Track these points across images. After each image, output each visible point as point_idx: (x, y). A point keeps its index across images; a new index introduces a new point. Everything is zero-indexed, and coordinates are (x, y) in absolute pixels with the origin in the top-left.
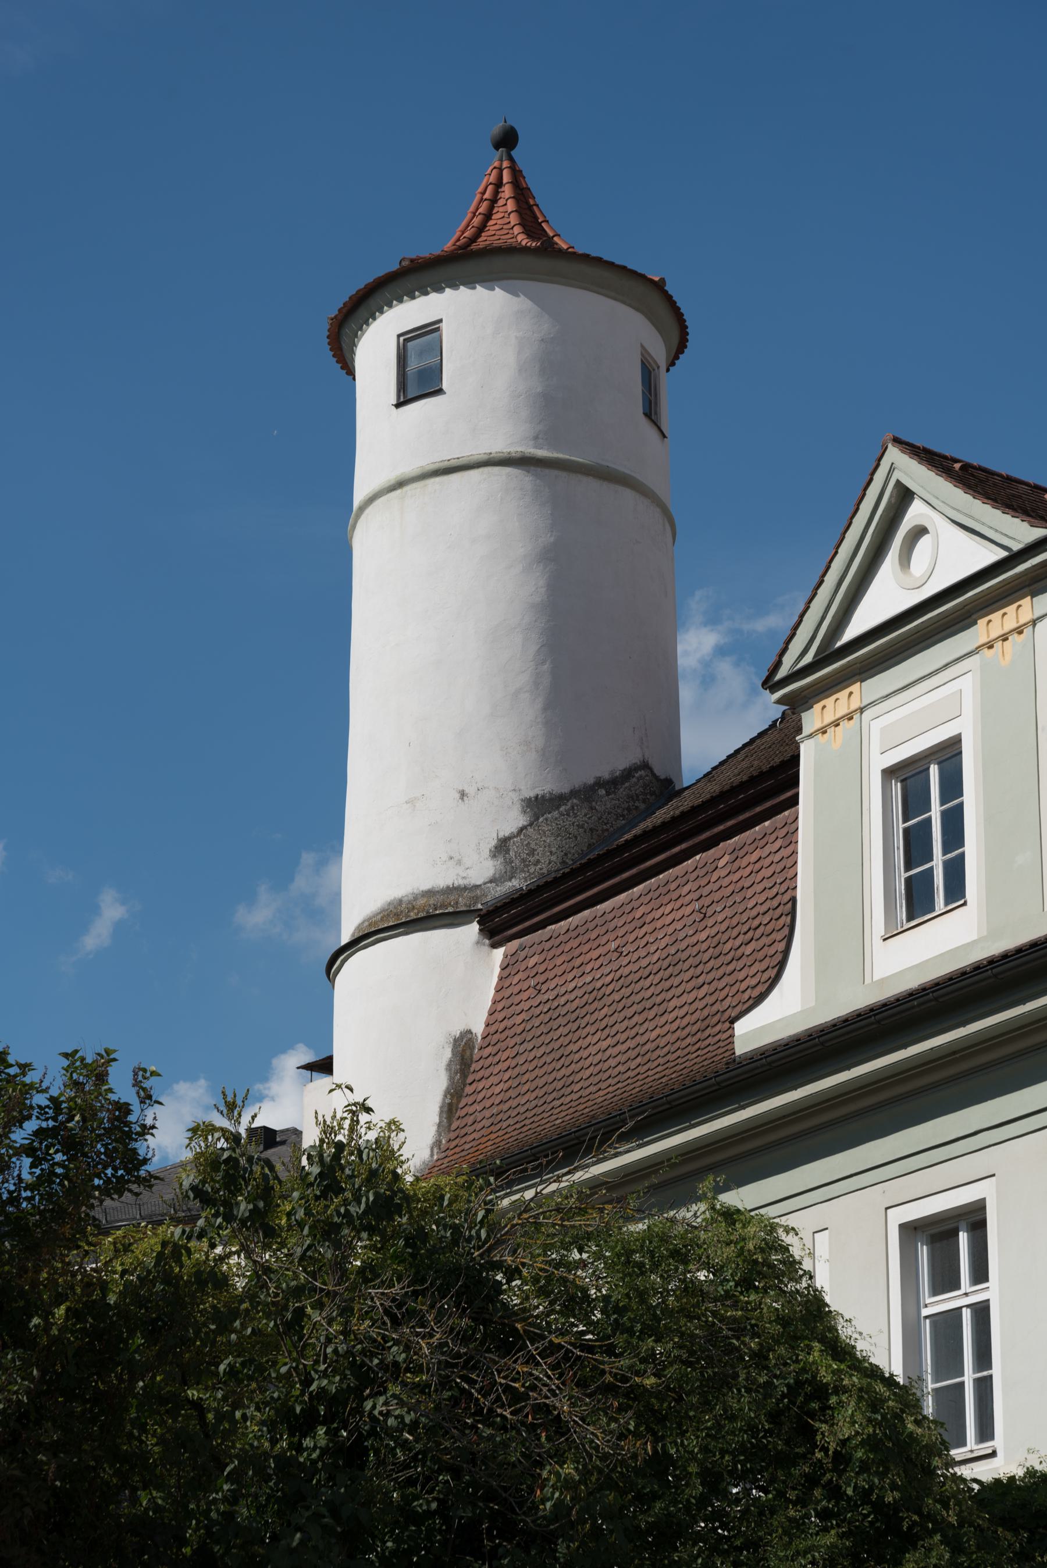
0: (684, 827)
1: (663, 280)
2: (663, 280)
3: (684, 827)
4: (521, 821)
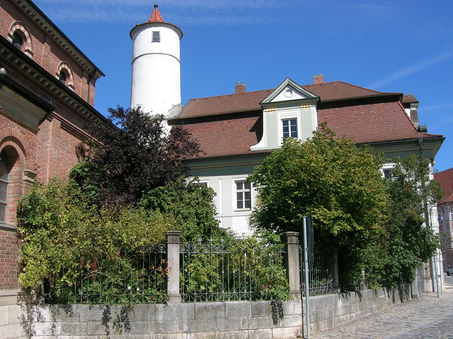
4: (172, 108)
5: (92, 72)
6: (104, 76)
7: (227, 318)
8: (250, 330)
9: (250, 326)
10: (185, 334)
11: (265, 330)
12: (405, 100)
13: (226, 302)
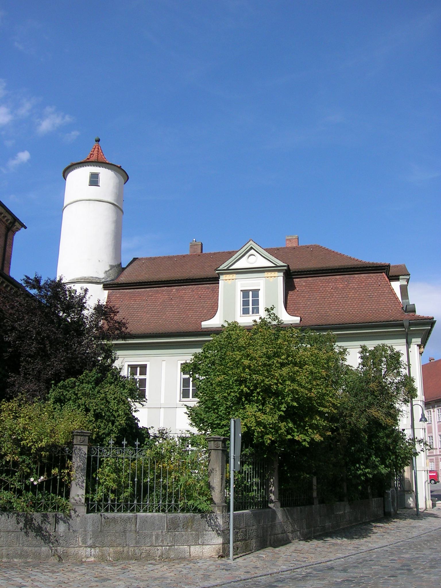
0: (165, 282)
1: (121, 166)
2: (121, 166)
3: (165, 282)
4: (109, 269)
5: (10, 223)
6: (26, 228)
7: (138, 532)
8: (164, 546)
9: (165, 542)
10: (89, 549)
11: (181, 547)
12: (392, 272)
13: (138, 514)
